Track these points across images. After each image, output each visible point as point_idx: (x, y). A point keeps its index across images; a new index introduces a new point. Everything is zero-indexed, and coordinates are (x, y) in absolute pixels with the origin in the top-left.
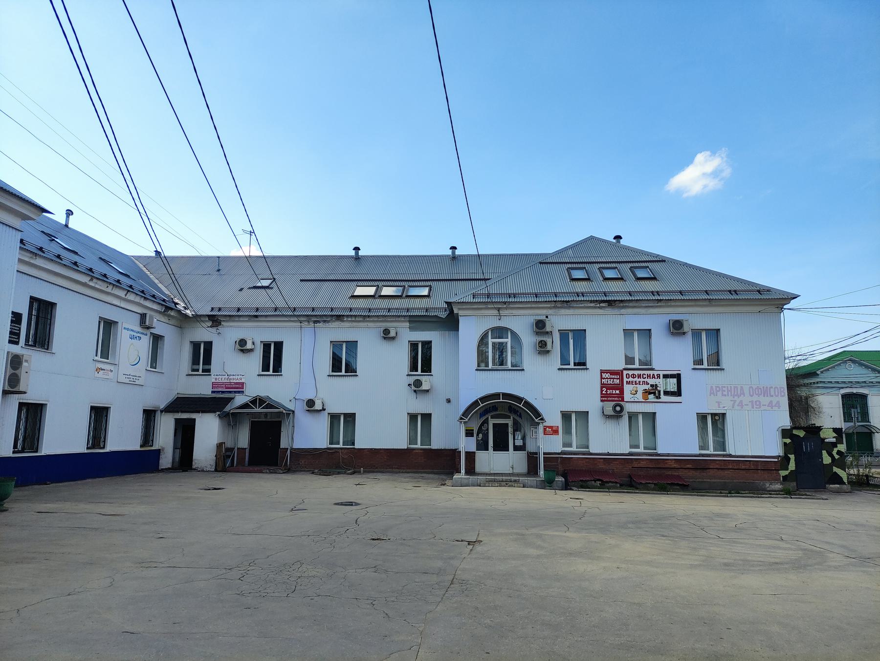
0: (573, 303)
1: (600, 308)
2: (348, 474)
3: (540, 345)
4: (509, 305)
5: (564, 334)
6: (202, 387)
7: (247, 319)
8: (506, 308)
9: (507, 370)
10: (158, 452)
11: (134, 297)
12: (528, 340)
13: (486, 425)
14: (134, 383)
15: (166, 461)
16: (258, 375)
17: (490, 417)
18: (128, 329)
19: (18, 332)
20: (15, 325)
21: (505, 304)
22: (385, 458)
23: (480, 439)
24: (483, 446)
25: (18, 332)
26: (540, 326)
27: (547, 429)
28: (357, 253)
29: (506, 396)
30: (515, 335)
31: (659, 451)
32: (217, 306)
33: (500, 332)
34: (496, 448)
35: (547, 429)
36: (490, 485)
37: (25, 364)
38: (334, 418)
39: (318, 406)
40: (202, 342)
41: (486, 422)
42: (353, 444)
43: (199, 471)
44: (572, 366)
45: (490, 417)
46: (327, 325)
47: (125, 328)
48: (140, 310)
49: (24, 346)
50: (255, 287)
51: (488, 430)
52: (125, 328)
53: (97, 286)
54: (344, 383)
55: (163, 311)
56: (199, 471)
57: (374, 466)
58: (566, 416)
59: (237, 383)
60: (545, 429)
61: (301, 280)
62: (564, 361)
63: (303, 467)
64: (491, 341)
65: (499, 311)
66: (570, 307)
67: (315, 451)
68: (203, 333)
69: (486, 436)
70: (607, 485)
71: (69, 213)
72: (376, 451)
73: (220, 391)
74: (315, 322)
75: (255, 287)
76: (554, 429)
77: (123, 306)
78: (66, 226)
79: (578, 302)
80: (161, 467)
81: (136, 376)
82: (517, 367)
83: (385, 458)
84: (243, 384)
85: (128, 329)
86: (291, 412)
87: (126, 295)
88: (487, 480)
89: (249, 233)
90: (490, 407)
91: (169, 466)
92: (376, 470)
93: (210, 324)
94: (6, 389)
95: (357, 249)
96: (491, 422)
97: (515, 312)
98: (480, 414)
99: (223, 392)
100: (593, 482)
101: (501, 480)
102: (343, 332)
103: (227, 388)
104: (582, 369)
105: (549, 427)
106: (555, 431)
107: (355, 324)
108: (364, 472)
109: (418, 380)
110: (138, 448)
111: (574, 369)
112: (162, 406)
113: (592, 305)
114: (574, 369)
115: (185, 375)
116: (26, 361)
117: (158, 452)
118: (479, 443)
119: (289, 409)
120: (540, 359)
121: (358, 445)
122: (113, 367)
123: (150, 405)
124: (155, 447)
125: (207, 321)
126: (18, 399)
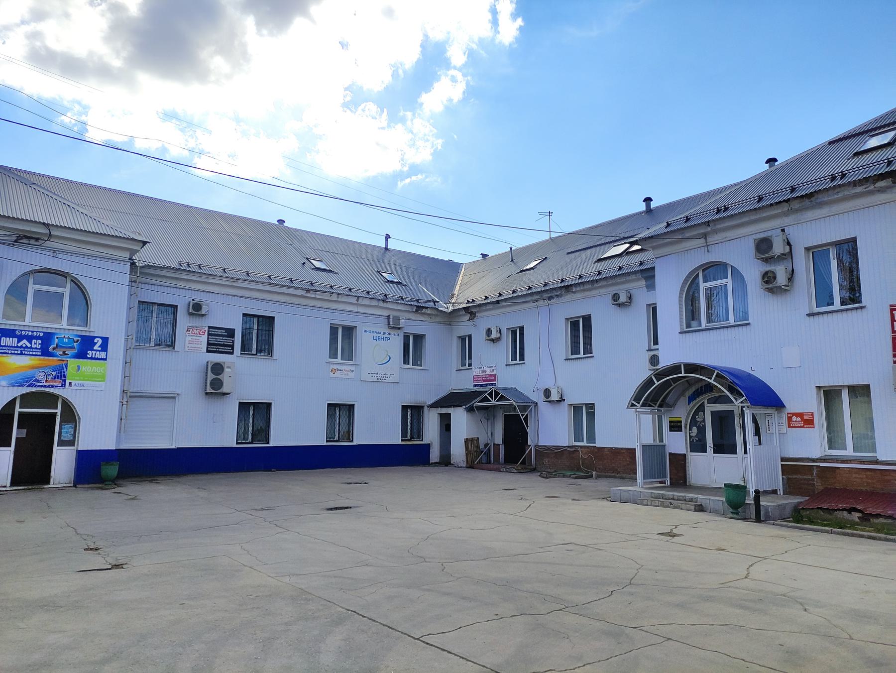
0: (820, 196)
1: (882, 190)
2: (573, 478)
3: (766, 279)
4: (715, 225)
5: (818, 253)
6: (465, 382)
7: (492, 307)
8: (716, 232)
9: (731, 327)
10: (428, 446)
11: (369, 301)
12: (752, 271)
13: (701, 413)
14: (385, 381)
15: (435, 455)
16: (506, 365)
17: (706, 402)
18: (370, 332)
19: (232, 344)
20: (226, 338)
21: (709, 225)
22: (628, 460)
23: (694, 435)
24: (698, 446)
25: (232, 344)
26: (763, 246)
27: (794, 418)
28: (648, 206)
29: (692, 368)
30: (737, 275)
31: (881, 457)
32: (470, 299)
33: (714, 269)
34: (718, 449)
35: (794, 418)
36: (649, 504)
37: (226, 370)
38: (577, 409)
39: (555, 397)
40: (466, 336)
41: (701, 408)
42: (874, 451)
43: (455, 467)
44: (837, 305)
45: (706, 402)
46: (560, 299)
47: (365, 331)
48: (386, 313)
49: (239, 355)
50: (522, 271)
51: (704, 421)
52: (365, 331)
53: (317, 297)
54: (582, 366)
55: (414, 310)
56: (455, 467)
57: (617, 470)
58: (830, 395)
59: (490, 376)
60: (790, 419)
61: (568, 254)
62: (824, 296)
63: (547, 467)
64: (703, 286)
65: (705, 238)
66: (821, 205)
67: (557, 449)
68: (464, 327)
69: (702, 431)
70: (876, 521)
71: (388, 237)
72: (618, 450)
73: (480, 385)
74: (550, 298)
75: (522, 271)
76: (805, 418)
77: (367, 312)
78: (386, 249)
79: (830, 192)
80: (431, 462)
81: (387, 375)
82: (743, 322)
83: (628, 460)
84: (494, 375)
85: (370, 332)
86: (533, 406)
87: (358, 301)
88: (653, 495)
89: (548, 214)
90: (702, 387)
91: (437, 460)
92: (619, 475)
93: (468, 317)
94: (208, 391)
95: (648, 200)
96: (709, 408)
97: (730, 234)
98: (689, 397)
99: (482, 385)
100: (845, 513)
101: (672, 497)
102: (575, 306)
103: (484, 381)
104: (857, 308)
105: (797, 415)
106: (809, 422)
107: (587, 293)
108: (598, 477)
109: (654, 355)
110: (323, 442)
111: (842, 311)
112: (429, 403)
113: (859, 189)
114: (842, 311)
115: (455, 370)
116: (228, 367)
117: (428, 446)
118: (693, 440)
119: (533, 401)
120: (774, 304)
121: (598, 444)
122: (354, 367)
123: (410, 401)
124: (426, 441)
125: (464, 315)
126: (237, 399)
